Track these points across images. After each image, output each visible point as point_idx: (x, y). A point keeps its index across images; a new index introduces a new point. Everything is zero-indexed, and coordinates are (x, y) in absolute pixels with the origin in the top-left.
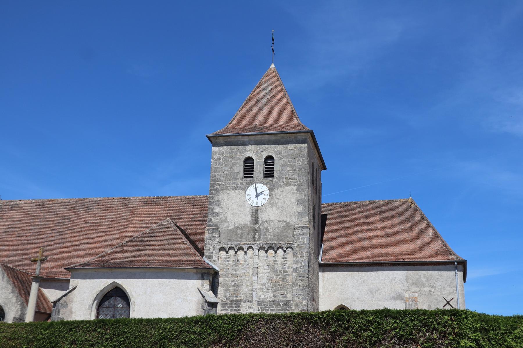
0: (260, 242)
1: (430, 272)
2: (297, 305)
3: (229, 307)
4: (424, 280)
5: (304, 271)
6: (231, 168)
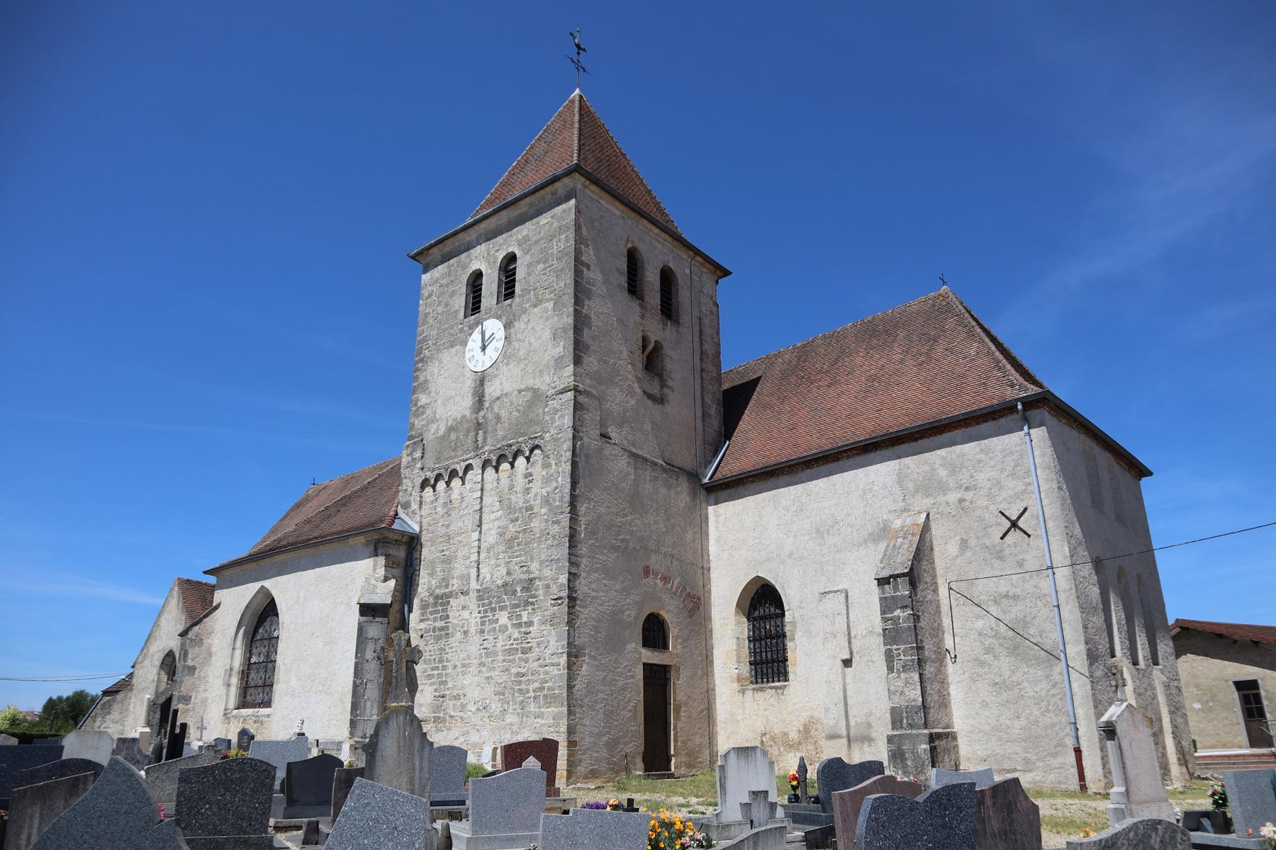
0: (486, 448)
1: (958, 449)
2: (548, 587)
3: (431, 613)
4: (943, 473)
5: (561, 500)
6: (447, 305)
